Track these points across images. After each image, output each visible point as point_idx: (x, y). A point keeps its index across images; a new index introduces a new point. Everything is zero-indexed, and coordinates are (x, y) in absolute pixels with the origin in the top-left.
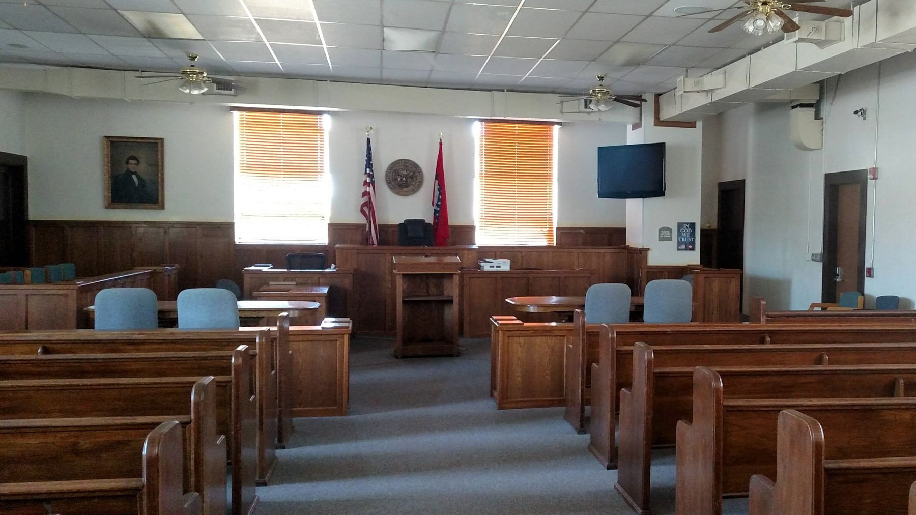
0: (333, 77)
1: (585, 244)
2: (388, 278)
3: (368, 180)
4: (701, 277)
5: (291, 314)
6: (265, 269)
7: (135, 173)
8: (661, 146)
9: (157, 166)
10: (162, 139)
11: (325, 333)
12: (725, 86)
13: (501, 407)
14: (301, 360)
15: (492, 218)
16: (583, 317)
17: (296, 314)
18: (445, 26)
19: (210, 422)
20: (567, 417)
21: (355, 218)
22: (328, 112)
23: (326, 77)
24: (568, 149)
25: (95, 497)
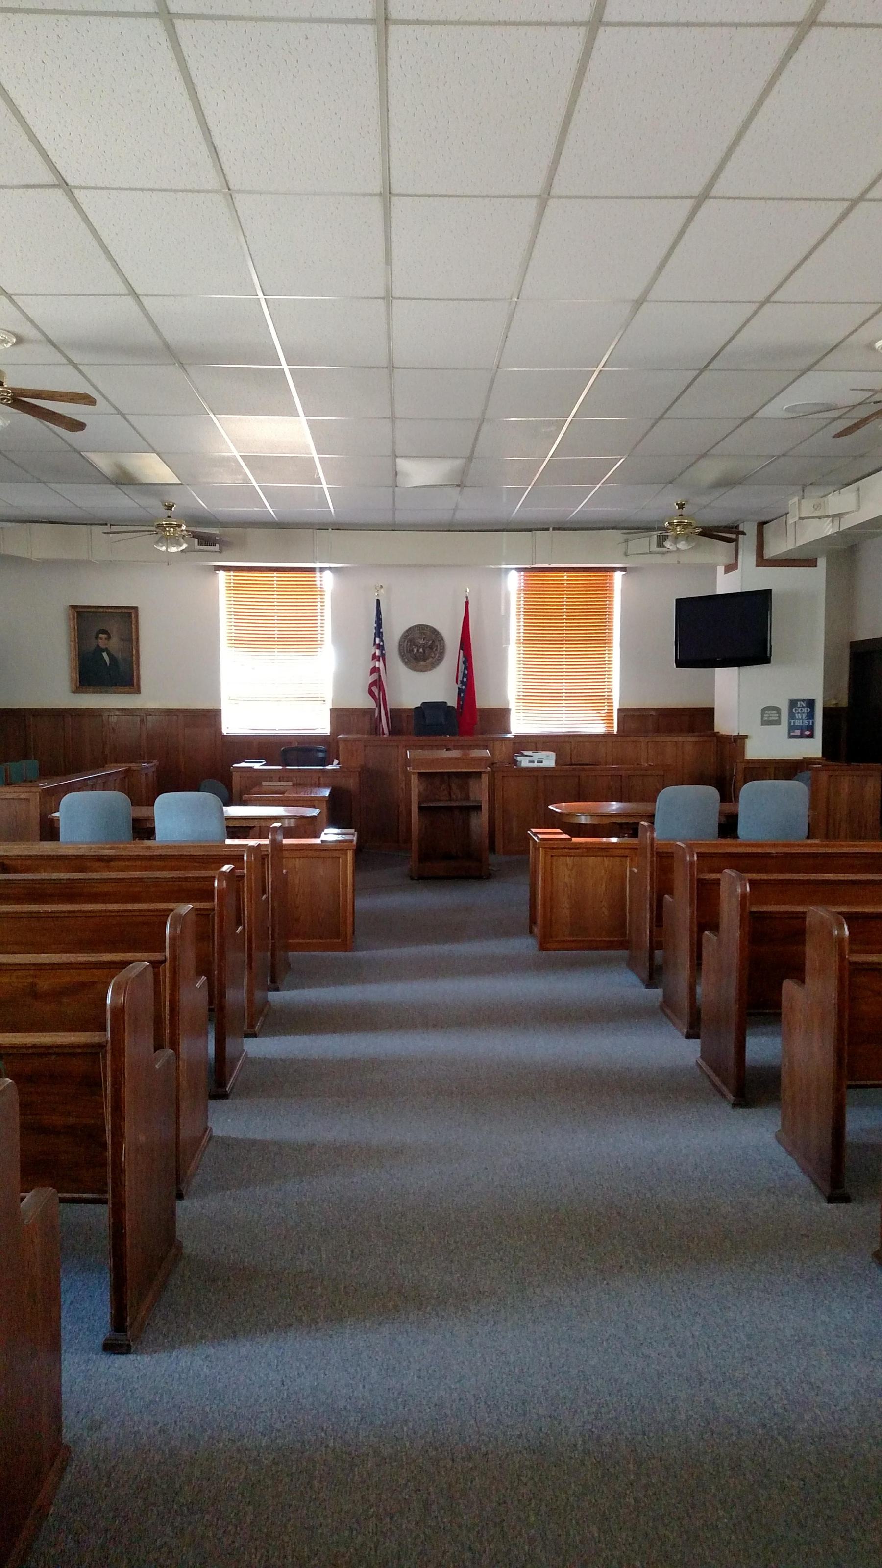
0: (334, 524)
1: (657, 730)
2: (401, 776)
3: (378, 653)
4: (824, 776)
5: (286, 823)
6: (257, 766)
7: (106, 650)
8: (766, 595)
9: (131, 640)
10: (136, 608)
11: (325, 848)
12: (859, 508)
13: (543, 947)
14: (297, 881)
15: (529, 698)
16: (652, 833)
17: (292, 823)
18: (473, 452)
19: (189, 958)
20: (632, 964)
21: (362, 701)
22: (330, 569)
23: (327, 524)
24: (634, 601)
25: (51, 1054)
